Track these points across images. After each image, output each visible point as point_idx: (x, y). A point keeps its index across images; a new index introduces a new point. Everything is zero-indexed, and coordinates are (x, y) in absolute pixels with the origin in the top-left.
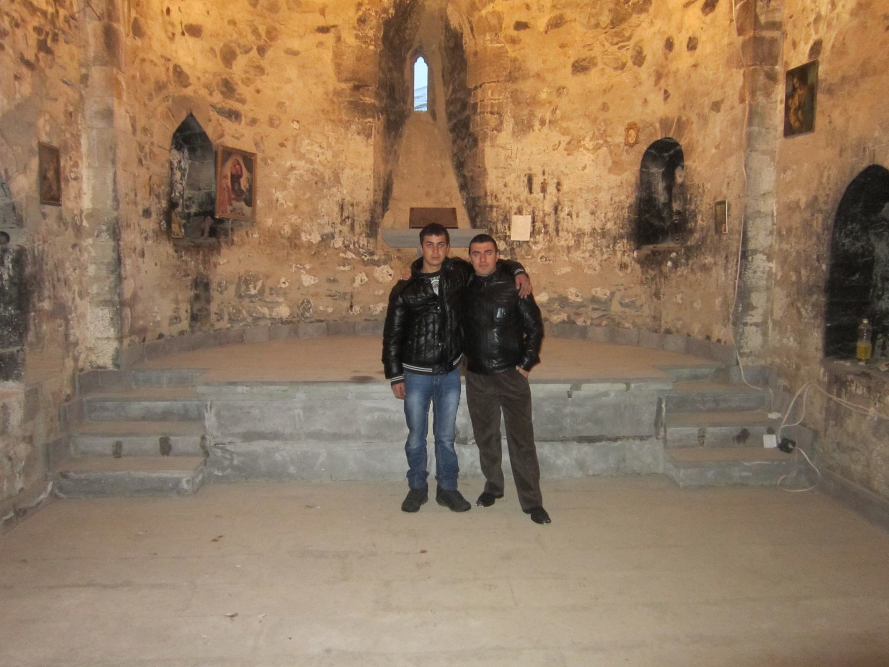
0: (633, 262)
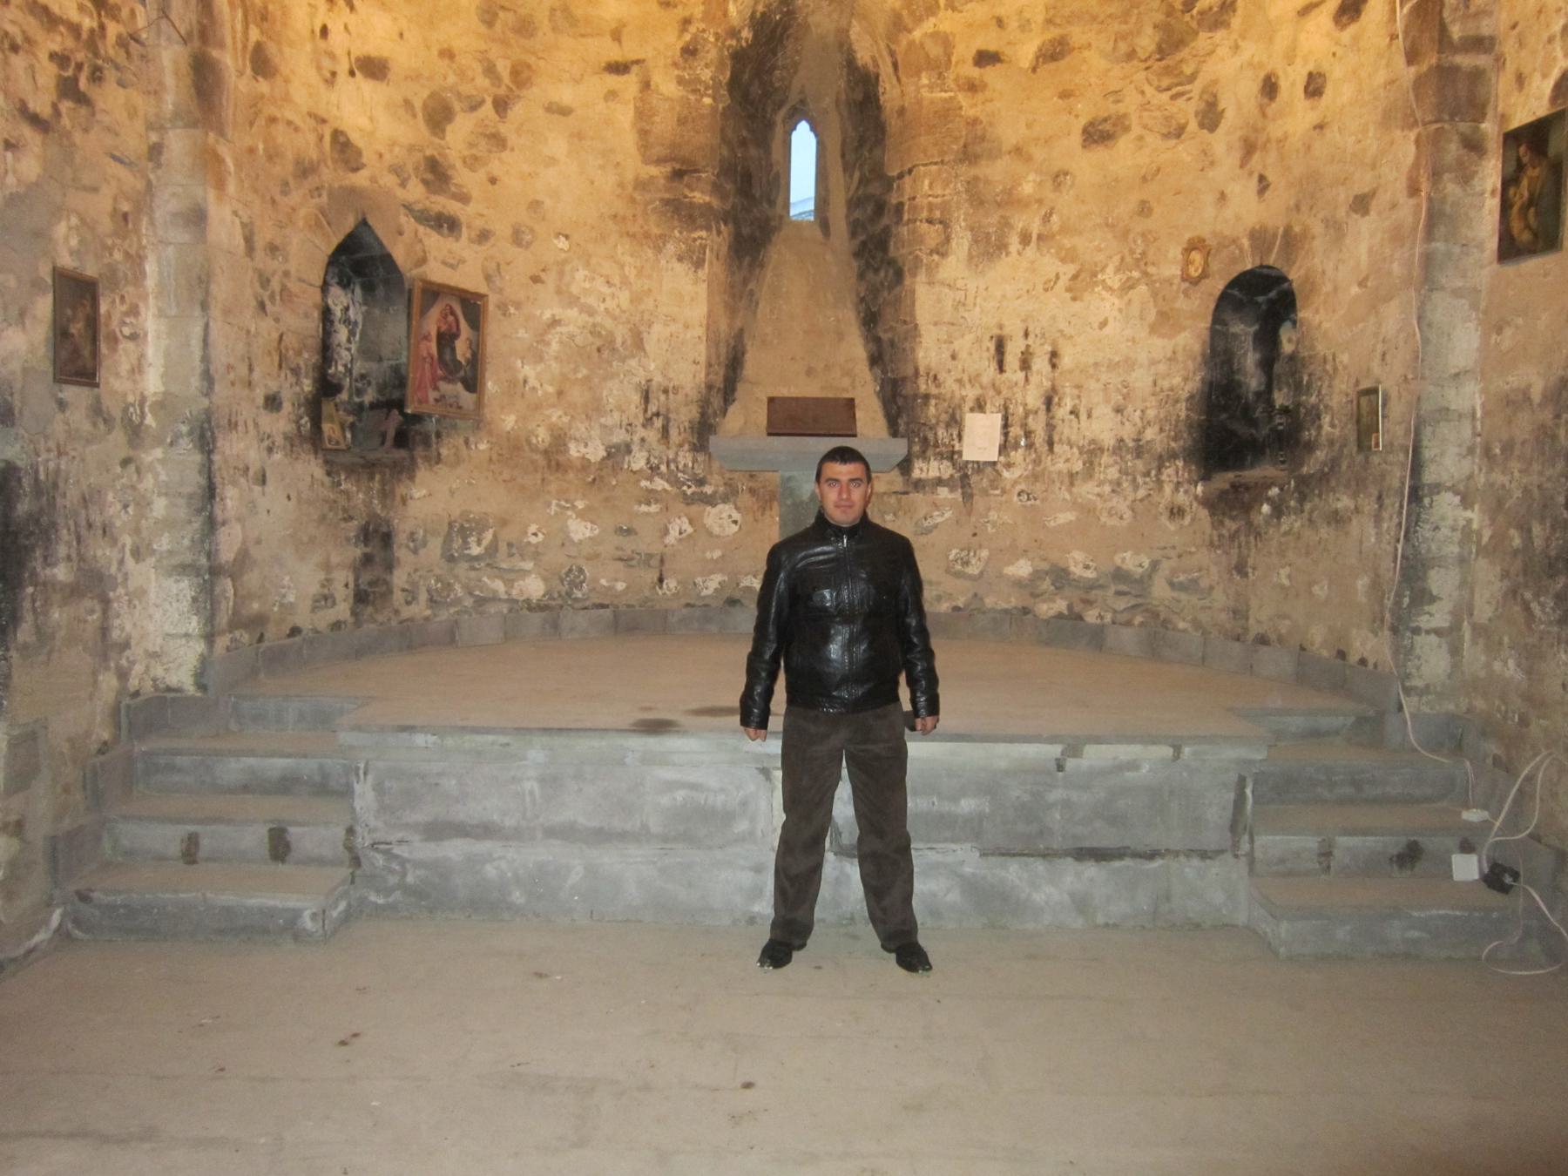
0: (1195, 504)
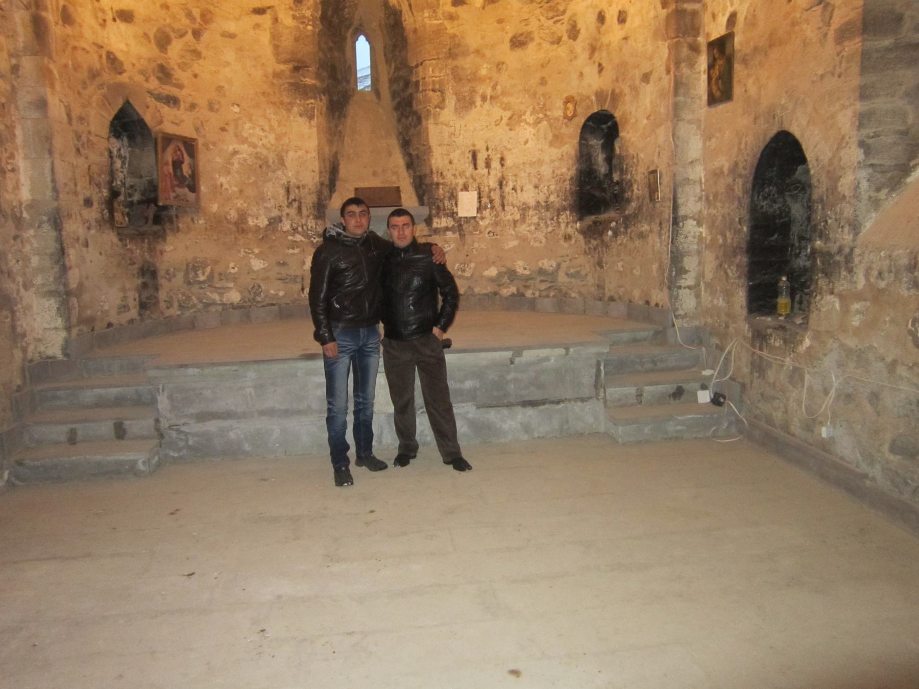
0: (576, 233)
